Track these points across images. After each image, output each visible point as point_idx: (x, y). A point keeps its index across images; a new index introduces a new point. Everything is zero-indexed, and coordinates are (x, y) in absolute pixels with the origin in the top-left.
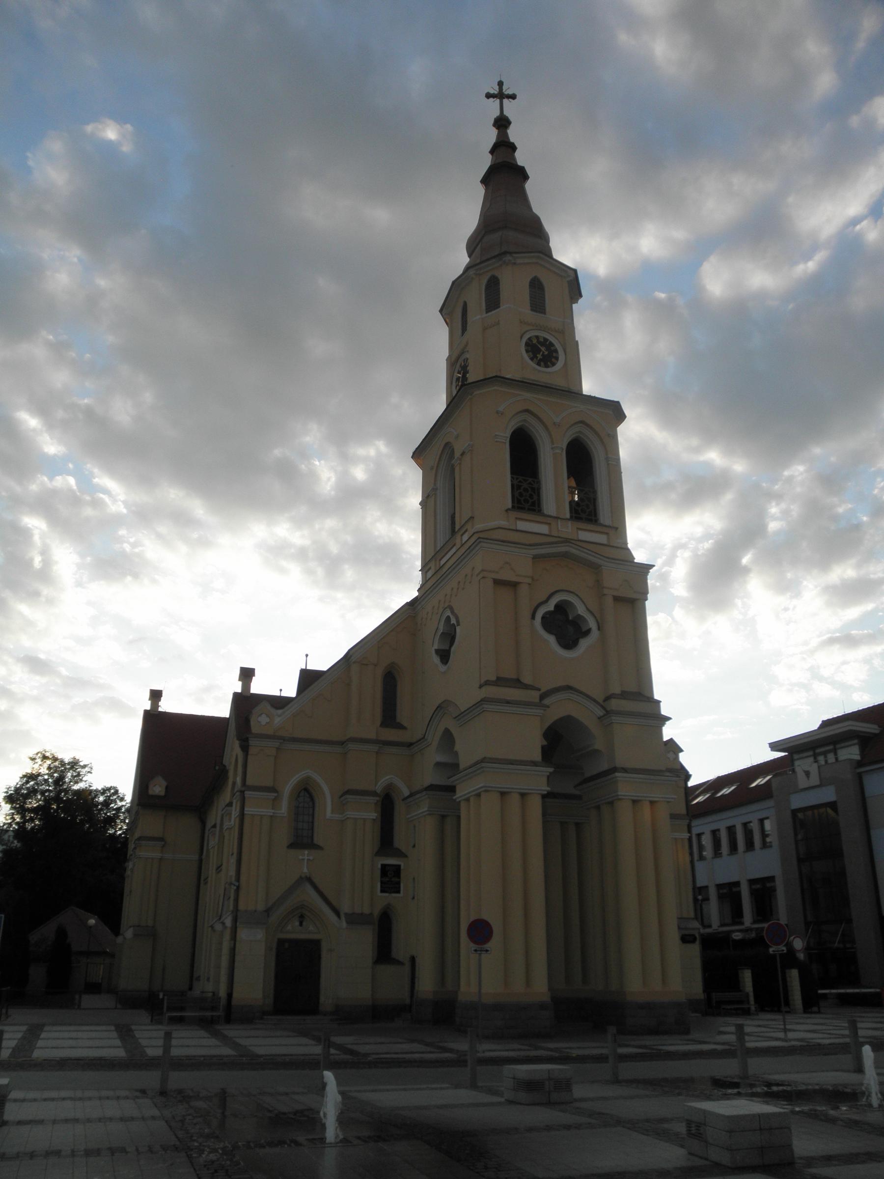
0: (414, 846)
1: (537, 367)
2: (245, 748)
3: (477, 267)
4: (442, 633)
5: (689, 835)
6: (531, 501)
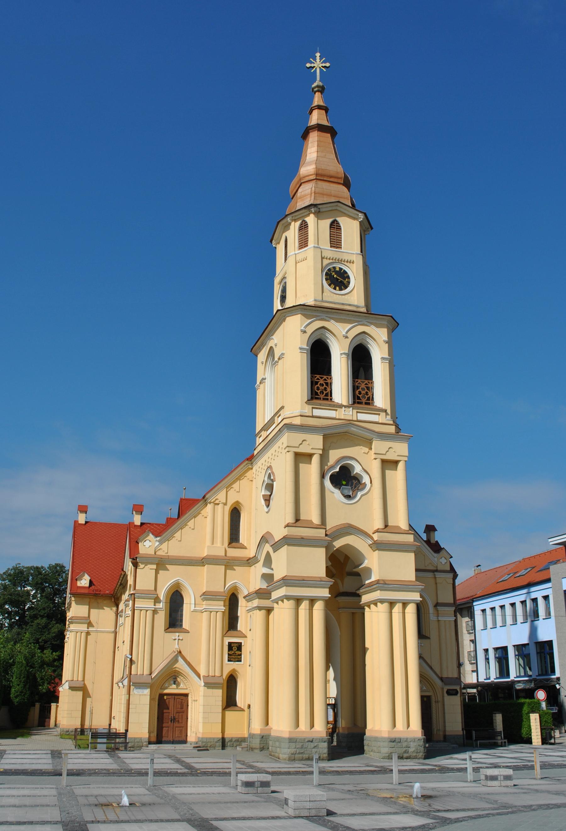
0: (250, 630)
1: (334, 291)
2: (135, 565)
3: (293, 215)
4: (267, 484)
5: (455, 618)
6: (325, 392)
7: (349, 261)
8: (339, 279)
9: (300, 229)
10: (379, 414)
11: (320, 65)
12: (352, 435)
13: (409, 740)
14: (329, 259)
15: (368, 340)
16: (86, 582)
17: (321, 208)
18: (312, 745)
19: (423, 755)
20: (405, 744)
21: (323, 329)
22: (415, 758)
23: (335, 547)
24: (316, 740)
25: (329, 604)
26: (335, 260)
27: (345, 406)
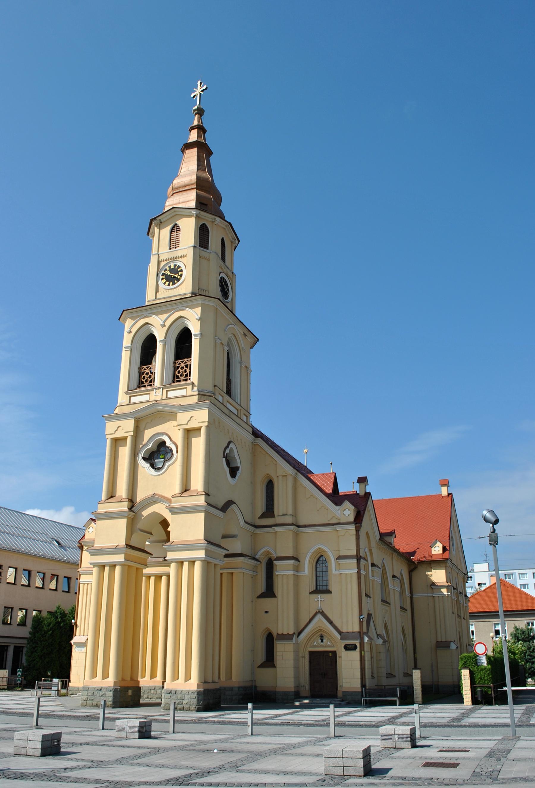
1: (169, 287)
7: (182, 256)
8: (172, 276)
10: (186, 388)
12: (164, 413)
13: (183, 693)
14: (166, 260)
15: (187, 323)
16: (439, 549)
17: (162, 219)
18: (101, 693)
19: (195, 707)
20: (179, 696)
21: (147, 325)
22: (189, 710)
23: (143, 516)
24: (104, 689)
25: (207, 564)
26: (171, 259)
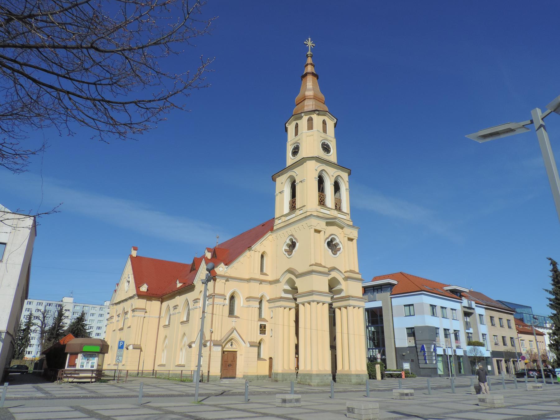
0: (105, 332)
9: (308, 120)
11: (311, 44)
16: (145, 289)
27: (334, 210)
